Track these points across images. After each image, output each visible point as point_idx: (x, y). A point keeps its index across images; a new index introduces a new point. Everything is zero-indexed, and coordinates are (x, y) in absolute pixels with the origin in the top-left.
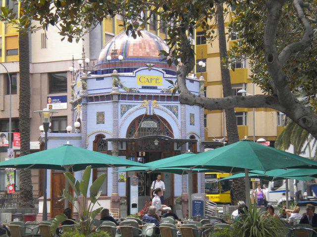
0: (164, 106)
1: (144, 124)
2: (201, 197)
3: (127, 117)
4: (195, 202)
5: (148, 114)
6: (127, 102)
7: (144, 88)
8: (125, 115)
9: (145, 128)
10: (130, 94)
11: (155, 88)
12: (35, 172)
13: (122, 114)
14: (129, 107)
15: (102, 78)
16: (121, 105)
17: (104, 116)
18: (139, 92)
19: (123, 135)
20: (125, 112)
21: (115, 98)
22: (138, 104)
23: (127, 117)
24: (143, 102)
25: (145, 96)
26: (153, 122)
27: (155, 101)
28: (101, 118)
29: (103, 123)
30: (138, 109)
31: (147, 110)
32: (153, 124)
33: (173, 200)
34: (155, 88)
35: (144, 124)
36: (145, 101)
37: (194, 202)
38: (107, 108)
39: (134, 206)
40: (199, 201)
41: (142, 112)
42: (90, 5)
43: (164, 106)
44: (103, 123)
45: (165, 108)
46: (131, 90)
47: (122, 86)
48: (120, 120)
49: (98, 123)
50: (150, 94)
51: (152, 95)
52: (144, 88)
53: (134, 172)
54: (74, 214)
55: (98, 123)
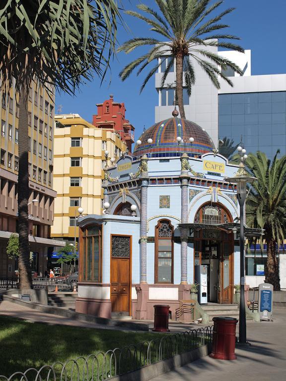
0: (226, 194)
1: (208, 211)
2: (269, 287)
3: (195, 202)
4: (264, 292)
5: (213, 201)
6: (193, 187)
7: (209, 173)
8: (193, 200)
9: (208, 216)
10: (199, 179)
11: (219, 175)
12: (169, 255)
13: (191, 200)
14: (197, 192)
15: (168, 160)
16: (190, 190)
17: (169, 200)
18: (205, 178)
19: (191, 220)
20: (193, 197)
21: (185, 182)
22: (204, 190)
23: (195, 202)
24: (208, 188)
25: (210, 182)
26: (214, 210)
27: (219, 189)
28: (165, 202)
29: (169, 207)
30: (205, 195)
31: (212, 197)
32: (214, 212)
33: (232, 290)
34: (219, 175)
35: (208, 211)
36: (210, 187)
37: (262, 292)
38: (174, 192)
39: (204, 295)
40: (268, 291)
41: (207, 199)
42: (82, 48)
43: (226, 194)
44: (169, 207)
45: (227, 197)
46: (198, 175)
47: (191, 170)
48: (189, 205)
49: (161, 207)
50: (216, 181)
51: (217, 181)
52: (209, 173)
53: (196, 260)
54: (133, 301)
55: (161, 207)
